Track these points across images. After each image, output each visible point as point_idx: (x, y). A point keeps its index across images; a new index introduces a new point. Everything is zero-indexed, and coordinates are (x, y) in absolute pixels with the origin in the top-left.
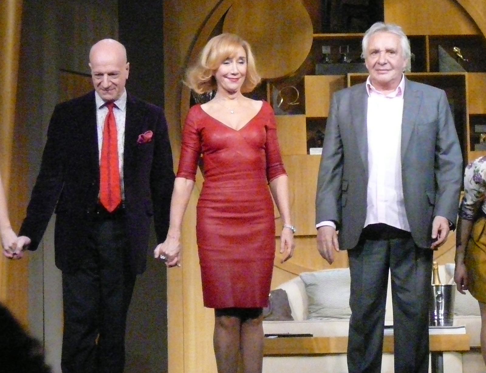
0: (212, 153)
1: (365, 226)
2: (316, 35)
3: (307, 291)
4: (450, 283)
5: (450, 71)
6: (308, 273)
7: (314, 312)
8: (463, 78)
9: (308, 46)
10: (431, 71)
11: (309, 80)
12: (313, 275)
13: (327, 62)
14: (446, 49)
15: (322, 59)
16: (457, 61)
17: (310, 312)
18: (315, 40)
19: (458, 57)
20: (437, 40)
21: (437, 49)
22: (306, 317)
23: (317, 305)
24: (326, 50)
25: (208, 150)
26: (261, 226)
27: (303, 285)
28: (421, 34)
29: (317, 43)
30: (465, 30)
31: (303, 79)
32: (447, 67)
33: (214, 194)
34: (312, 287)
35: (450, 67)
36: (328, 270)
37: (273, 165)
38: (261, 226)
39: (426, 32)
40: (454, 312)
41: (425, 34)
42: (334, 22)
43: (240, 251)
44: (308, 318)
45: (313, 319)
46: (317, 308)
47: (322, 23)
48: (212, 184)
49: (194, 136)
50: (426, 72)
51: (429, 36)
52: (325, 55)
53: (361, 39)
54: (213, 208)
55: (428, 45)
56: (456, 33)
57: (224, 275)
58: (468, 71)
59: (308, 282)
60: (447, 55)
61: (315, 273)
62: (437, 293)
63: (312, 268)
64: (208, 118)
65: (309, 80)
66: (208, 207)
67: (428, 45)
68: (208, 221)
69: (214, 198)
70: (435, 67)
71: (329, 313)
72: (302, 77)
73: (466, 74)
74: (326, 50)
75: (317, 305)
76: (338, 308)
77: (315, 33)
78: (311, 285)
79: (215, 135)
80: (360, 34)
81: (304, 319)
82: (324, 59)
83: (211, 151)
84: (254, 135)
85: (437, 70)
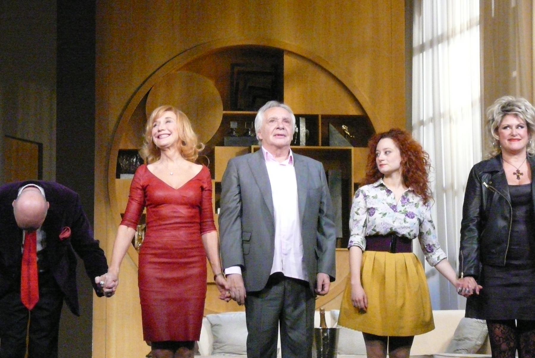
0: (154, 207)
1: (272, 273)
2: (224, 112)
3: (212, 330)
4: (334, 327)
5: (340, 146)
6: (214, 315)
7: (218, 348)
8: (349, 151)
9: (218, 122)
10: (322, 145)
11: (218, 149)
12: (218, 317)
13: (234, 136)
14: (335, 126)
15: (230, 132)
16: (345, 137)
17: (214, 349)
18: (225, 117)
19: (346, 134)
20: (329, 119)
21: (329, 126)
22: (211, 352)
23: (221, 343)
24: (233, 125)
25: (151, 204)
26: (195, 271)
27: (210, 325)
28: (315, 113)
29: (226, 119)
30: (352, 111)
31: (214, 149)
32: (336, 142)
33: (153, 243)
34: (216, 327)
35: (338, 142)
36: (232, 313)
37: (205, 220)
38: (195, 271)
39: (318, 111)
40: (338, 351)
41: (318, 113)
42: (241, 101)
43: (174, 291)
44: (213, 353)
45: (217, 355)
46: (221, 345)
47: (231, 102)
48: (153, 234)
49: (139, 192)
50: (318, 145)
51: (322, 116)
52: (232, 129)
53: (254, 116)
54: (152, 254)
55: (320, 124)
56: (344, 113)
57: (161, 312)
58: (354, 147)
59: (214, 323)
60: (337, 132)
61: (220, 315)
62: (323, 335)
63: (216, 311)
64: (152, 177)
65: (218, 149)
66: (148, 254)
67: (320, 124)
68: (148, 266)
69: (154, 246)
70: (326, 142)
71: (227, 348)
72: (213, 147)
73: (353, 148)
74: (233, 125)
75: (221, 343)
76: (238, 346)
77: (224, 110)
78: (215, 325)
79: (157, 192)
80: (255, 112)
81: (209, 354)
82: (232, 133)
83: (153, 206)
84: (191, 194)
85: (328, 145)
